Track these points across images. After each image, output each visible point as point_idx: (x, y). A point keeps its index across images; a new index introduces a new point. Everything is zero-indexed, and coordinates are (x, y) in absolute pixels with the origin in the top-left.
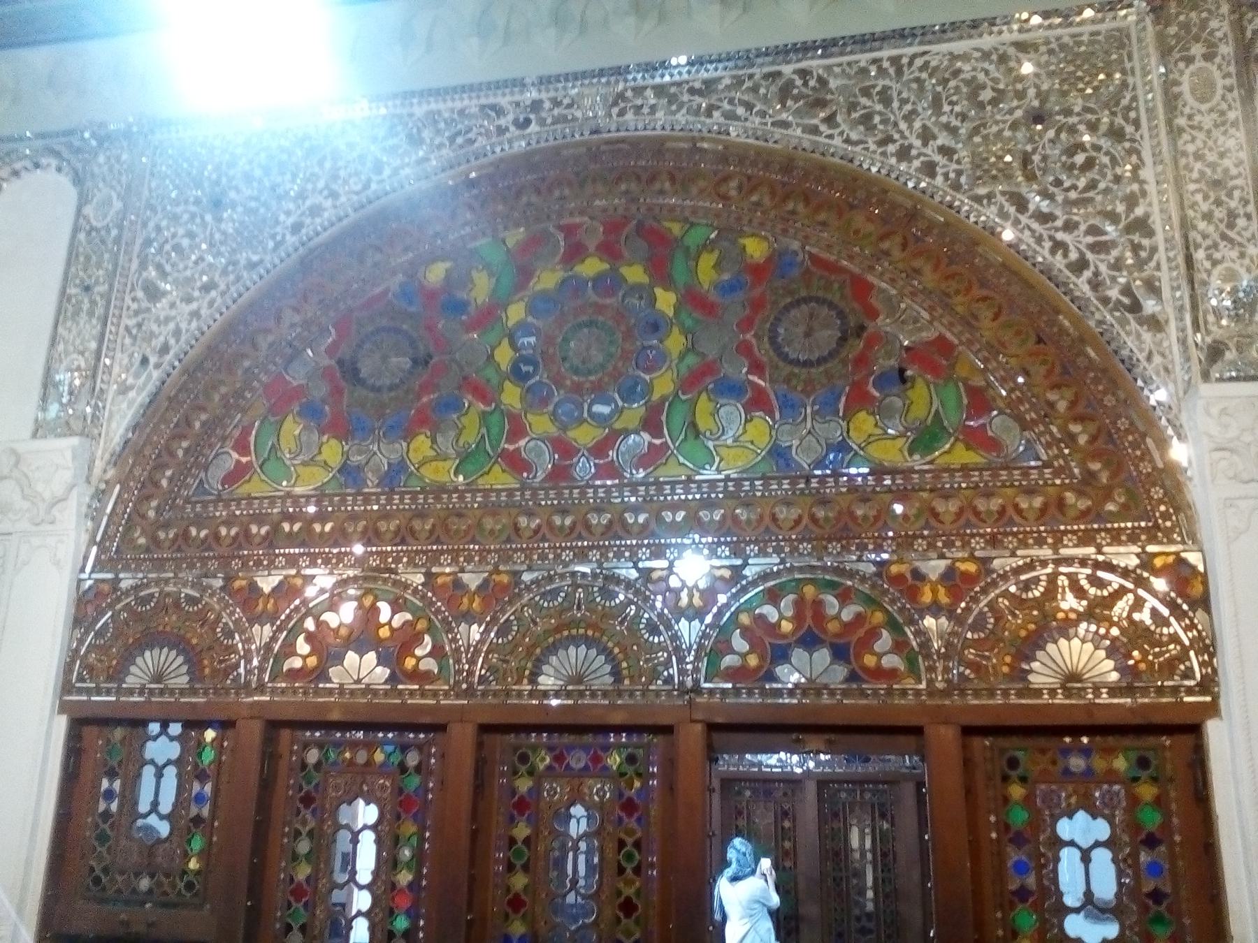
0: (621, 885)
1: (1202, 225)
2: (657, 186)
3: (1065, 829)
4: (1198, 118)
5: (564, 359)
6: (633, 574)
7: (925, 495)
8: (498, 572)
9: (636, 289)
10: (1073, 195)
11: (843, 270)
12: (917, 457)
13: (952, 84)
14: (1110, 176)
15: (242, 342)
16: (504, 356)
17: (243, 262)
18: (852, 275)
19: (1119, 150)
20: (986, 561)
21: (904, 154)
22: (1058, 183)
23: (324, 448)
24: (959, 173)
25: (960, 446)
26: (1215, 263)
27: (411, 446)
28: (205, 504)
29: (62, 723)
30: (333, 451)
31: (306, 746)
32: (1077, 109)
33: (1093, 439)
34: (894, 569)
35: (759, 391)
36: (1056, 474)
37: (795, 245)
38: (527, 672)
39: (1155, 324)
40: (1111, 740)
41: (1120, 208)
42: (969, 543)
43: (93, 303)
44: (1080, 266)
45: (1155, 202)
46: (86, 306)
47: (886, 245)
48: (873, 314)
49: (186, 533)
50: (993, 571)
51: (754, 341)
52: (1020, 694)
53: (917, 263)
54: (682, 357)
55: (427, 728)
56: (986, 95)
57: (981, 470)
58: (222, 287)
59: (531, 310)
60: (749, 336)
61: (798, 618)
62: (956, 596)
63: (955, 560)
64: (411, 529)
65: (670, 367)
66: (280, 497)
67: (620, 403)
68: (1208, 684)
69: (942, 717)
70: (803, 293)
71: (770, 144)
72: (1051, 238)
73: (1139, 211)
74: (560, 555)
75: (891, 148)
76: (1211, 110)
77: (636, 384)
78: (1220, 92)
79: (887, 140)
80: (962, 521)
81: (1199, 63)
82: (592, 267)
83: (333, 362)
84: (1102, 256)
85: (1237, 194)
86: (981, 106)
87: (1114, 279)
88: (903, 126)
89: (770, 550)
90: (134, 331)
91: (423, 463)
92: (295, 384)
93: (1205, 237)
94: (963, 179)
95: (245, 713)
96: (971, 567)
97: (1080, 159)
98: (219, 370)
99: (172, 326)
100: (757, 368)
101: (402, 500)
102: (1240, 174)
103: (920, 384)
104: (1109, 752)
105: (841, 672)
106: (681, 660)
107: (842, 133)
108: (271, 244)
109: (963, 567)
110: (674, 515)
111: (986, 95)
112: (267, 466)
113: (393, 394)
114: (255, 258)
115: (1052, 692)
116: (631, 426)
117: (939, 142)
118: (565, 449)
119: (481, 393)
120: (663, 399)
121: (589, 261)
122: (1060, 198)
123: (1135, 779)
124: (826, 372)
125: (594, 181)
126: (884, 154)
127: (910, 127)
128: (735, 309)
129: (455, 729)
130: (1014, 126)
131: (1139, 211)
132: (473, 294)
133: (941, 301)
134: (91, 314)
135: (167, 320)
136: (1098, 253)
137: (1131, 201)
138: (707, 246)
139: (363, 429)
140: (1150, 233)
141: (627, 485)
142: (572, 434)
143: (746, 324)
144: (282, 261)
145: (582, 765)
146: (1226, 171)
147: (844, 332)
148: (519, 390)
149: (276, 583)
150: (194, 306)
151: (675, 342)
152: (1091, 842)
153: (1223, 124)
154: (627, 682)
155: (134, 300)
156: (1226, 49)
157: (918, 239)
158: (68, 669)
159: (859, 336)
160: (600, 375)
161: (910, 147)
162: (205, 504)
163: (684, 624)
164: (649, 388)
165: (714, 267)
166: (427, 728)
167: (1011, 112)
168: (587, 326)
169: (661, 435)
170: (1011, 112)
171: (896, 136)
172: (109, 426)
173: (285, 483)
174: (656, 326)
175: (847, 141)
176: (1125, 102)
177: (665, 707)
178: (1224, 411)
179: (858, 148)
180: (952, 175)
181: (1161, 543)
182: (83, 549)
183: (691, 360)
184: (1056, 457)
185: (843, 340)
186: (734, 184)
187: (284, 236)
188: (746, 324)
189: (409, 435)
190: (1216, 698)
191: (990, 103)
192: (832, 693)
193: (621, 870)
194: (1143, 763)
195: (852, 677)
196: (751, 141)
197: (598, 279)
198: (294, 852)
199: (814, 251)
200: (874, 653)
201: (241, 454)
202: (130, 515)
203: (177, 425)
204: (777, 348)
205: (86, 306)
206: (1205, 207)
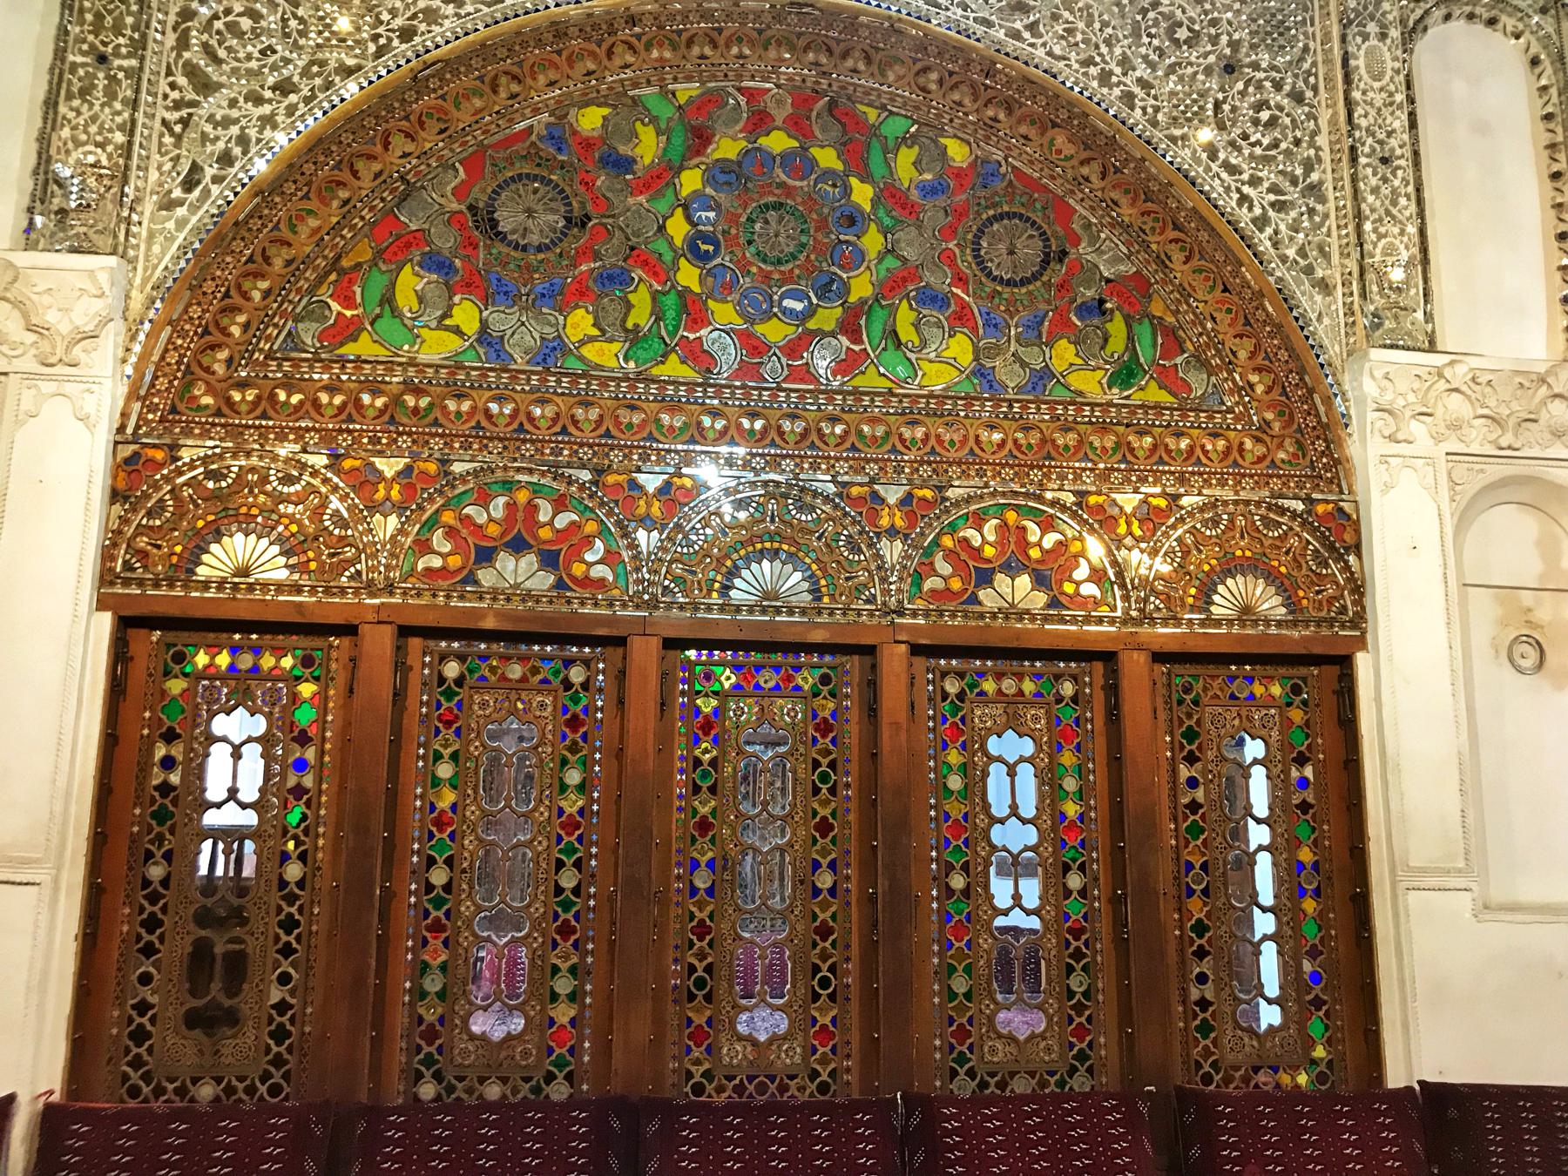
0: (816, 805)
1: (1371, 199)
2: (850, 63)
3: (994, 746)
4: (1371, 94)
5: (750, 243)
6: (831, 488)
7: (1121, 429)
8: (681, 476)
9: (829, 173)
10: (1258, 151)
11: (1045, 188)
12: (1115, 390)
13: (1151, 15)
14: (1290, 139)
15: (338, 166)
16: (678, 228)
17: (333, 64)
18: (1056, 195)
19: (1300, 112)
20: (1177, 497)
21: (1105, 78)
22: (1245, 137)
23: (455, 310)
24: (1157, 109)
25: (1153, 384)
26: (1380, 237)
27: (569, 320)
28: (296, 363)
29: (106, 620)
30: (466, 315)
31: (443, 658)
32: (1264, 65)
33: (1269, 390)
34: (1093, 500)
35: (964, 306)
36: (1237, 419)
37: (998, 156)
38: (717, 585)
39: (1324, 287)
40: (1270, 670)
41: (1299, 171)
42: (303, 437)
43: (112, 79)
44: (1261, 222)
45: (1329, 170)
46: (101, 82)
47: (1085, 171)
48: (1076, 241)
49: (272, 397)
50: (1182, 508)
51: (957, 251)
52: (1203, 623)
53: (1115, 195)
54: (881, 258)
55: (594, 641)
56: (1182, 34)
57: (1171, 409)
58: (306, 92)
59: (709, 179)
60: (951, 245)
61: (1000, 544)
62: (911, 518)
63: (1148, 495)
64: (573, 416)
65: (868, 268)
66: (400, 364)
67: (815, 301)
68: (1359, 620)
69: (643, 627)
70: (1006, 208)
71: (972, 41)
72: (1238, 190)
73: (1315, 177)
74: (395, 441)
75: (1093, 71)
76: (1381, 89)
77: (833, 281)
78: (1389, 73)
79: (1089, 62)
80: (1155, 458)
81: (1373, 42)
82: (778, 142)
83: (463, 207)
84: (1282, 216)
85: (1400, 173)
86: (1176, 42)
87: (1291, 239)
88: (1104, 49)
89: (973, 473)
90: (178, 128)
91: (582, 343)
92: (413, 227)
93: (1373, 210)
94: (1160, 117)
95: (371, 617)
96: (1162, 503)
97: (1265, 115)
98: (306, 197)
99: (235, 130)
100: (960, 280)
101: (559, 382)
102: (1402, 156)
103: (1118, 316)
104: (280, 652)
105: (1041, 599)
106: (883, 580)
107: (1044, 45)
108: (372, 48)
109: (1154, 501)
110: (289, 396)
111: (1182, 34)
112: (379, 324)
113: (541, 256)
114: (351, 62)
115: (1230, 622)
116: (827, 328)
117: (1138, 73)
118: (754, 346)
119: (654, 267)
120: (863, 301)
121: (775, 134)
122: (1246, 152)
123: (1289, 704)
124: (1030, 293)
125: (779, 43)
126: (1086, 74)
127: (1111, 52)
128: (933, 215)
129: (636, 643)
130: (1208, 71)
131: (1315, 177)
132: (638, 151)
133: (1135, 237)
134: (111, 95)
135: (227, 122)
136: (1279, 211)
137: (1309, 166)
138: (905, 140)
139: (506, 293)
140: (1322, 200)
141: (822, 392)
142: (759, 329)
143: (950, 232)
144: (389, 72)
145: (771, 684)
146: (1392, 150)
147: (1047, 255)
148: (698, 271)
149: (401, 466)
150: (266, 109)
151: (872, 241)
152: (244, 737)
153: (1391, 104)
154: (826, 599)
155: (173, 86)
156: (1395, 33)
157: (1117, 171)
158: (107, 555)
159: (1061, 261)
160: (790, 266)
161: (1111, 73)
162: (296, 363)
163: (884, 542)
164: (846, 289)
165: (914, 164)
166: (594, 641)
167: (1206, 55)
168: (774, 209)
169: (858, 341)
170: (1206, 55)
171: (1098, 59)
172: (149, 249)
173: (406, 347)
174: (853, 220)
175: (1050, 54)
176: (1306, 66)
177: (865, 622)
178: (1387, 377)
179: (1062, 64)
180: (1150, 110)
181: (1322, 492)
182: (121, 403)
183: (891, 262)
184: (1237, 404)
185: (1046, 262)
186: (934, 76)
187: (390, 40)
188: (950, 232)
189: (564, 309)
190: (1364, 633)
191: (1185, 42)
192: (1033, 619)
193: (816, 791)
194: (307, 662)
195: (560, 585)
196: (952, 34)
197: (786, 156)
198: (434, 776)
199: (1016, 163)
200: (1071, 581)
201: (854, 342)
202: (188, 366)
203: (251, 260)
204: (980, 262)
205: (101, 82)
206: (1374, 181)
